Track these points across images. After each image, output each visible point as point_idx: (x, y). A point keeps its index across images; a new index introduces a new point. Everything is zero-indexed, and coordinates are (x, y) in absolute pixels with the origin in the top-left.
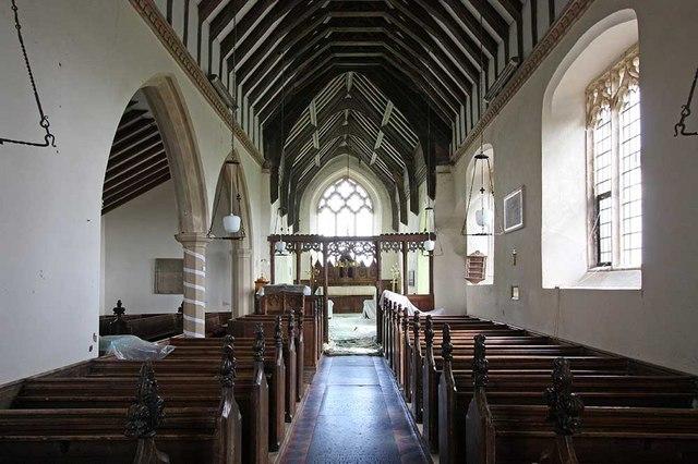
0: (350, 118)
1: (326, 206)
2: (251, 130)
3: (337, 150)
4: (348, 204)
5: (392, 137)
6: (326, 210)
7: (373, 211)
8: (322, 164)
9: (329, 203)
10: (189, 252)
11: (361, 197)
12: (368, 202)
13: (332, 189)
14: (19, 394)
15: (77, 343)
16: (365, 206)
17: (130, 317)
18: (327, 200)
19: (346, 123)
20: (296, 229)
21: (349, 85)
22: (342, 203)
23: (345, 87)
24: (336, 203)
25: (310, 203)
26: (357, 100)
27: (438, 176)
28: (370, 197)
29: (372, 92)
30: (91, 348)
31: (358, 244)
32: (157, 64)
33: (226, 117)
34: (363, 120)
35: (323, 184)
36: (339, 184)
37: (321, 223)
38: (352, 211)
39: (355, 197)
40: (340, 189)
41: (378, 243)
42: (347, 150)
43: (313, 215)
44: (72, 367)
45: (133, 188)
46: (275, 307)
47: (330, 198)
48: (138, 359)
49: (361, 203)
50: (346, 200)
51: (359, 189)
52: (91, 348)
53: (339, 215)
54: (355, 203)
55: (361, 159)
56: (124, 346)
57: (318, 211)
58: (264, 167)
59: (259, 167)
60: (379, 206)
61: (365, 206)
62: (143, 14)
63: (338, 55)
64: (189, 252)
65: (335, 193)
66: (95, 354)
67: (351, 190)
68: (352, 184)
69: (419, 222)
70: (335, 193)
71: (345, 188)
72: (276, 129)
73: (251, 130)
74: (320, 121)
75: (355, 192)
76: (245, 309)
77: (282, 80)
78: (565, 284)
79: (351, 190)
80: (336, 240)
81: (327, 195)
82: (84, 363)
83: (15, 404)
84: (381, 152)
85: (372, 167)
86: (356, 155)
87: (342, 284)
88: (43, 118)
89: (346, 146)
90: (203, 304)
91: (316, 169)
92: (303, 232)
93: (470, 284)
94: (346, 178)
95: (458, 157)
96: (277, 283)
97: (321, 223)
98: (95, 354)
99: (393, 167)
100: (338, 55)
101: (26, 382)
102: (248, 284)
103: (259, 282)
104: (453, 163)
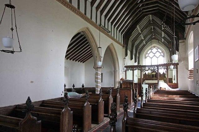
0: (154, 28)
1: (148, 56)
2: (118, 37)
3: (151, 39)
4: (155, 55)
5: (166, 32)
6: (148, 58)
7: (164, 56)
8: (146, 44)
9: (149, 55)
10: (97, 71)
11: (160, 53)
12: (162, 54)
13: (150, 51)
14: (42, 103)
15: (59, 93)
16: (161, 55)
17: (85, 88)
18: (148, 54)
19: (153, 30)
20: (139, 63)
21: (151, 19)
22: (153, 55)
23: (150, 20)
24: (151, 55)
25: (142, 57)
26: (154, 23)
27: (180, 44)
28: (163, 52)
29: (158, 21)
30: (62, 95)
31: (147, 67)
32: (79, 25)
33: (108, 35)
34: (157, 29)
35: (161, 48)
36: (152, 49)
37: (146, 62)
38: (156, 57)
39: (158, 53)
40: (152, 51)
41: (167, 66)
42: (154, 38)
43: (144, 59)
44: (56, 99)
45: (88, 57)
46: (125, 86)
47: (149, 54)
48: (74, 98)
49: (160, 54)
50: (154, 56)
51: (159, 50)
52: (62, 95)
53: (159, 58)
54: (158, 54)
55: (159, 40)
56: (70, 95)
57: (146, 58)
58: (123, 47)
59: (122, 47)
60: (166, 55)
61: (161, 55)
62: (77, 14)
63: (144, 11)
64: (97, 71)
65: (151, 52)
66: (63, 96)
67: (157, 50)
68: (156, 49)
69: (176, 57)
70: (151, 52)
71: (154, 50)
72: (126, 37)
73: (118, 37)
74: (142, 31)
75: (158, 51)
76: (117, 86)
77: (127, 21)
78: (129, 79)
79: (157, 50)
80: (152, 66)
81: (148, 53)
82: (59, 98)
83: (41, 105)
84: (164, 38)
85: (163, 43)
86: (157, 39)
87: (153, 80)
88: (20, 46)
89: (153, 37)
90: (100, 85)
91: (144, 46)
92: (141, 64)
93: (189, 79)
94: (154, 47)
95: (186, 36)
96: (127, 79)
97: (146, 62)
98: (63, 96)
99: (168, 42)
100: (144, 11)
101: (43, 101)
102: (118, 80)
103: (122, 79)
104: (185, 39)
